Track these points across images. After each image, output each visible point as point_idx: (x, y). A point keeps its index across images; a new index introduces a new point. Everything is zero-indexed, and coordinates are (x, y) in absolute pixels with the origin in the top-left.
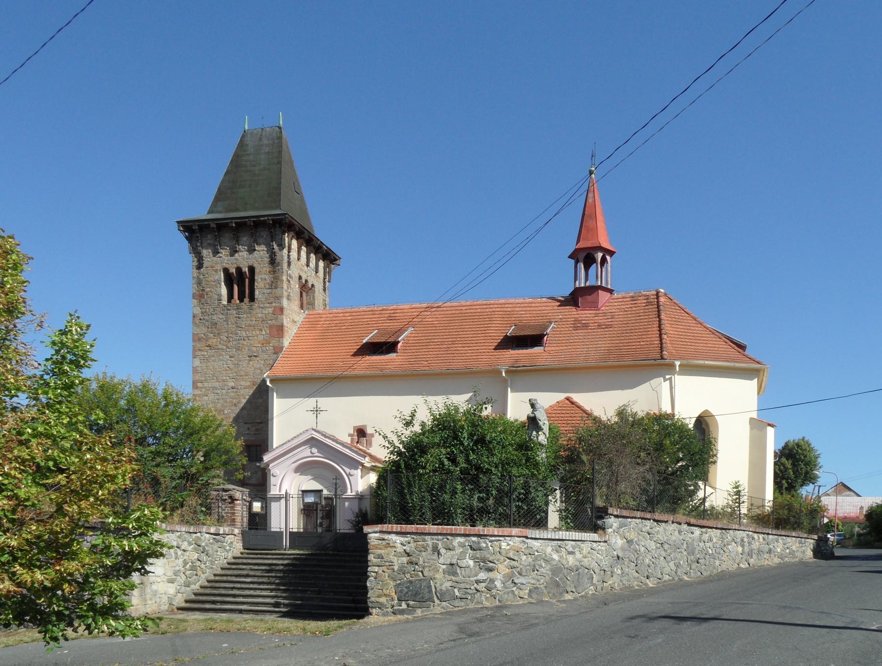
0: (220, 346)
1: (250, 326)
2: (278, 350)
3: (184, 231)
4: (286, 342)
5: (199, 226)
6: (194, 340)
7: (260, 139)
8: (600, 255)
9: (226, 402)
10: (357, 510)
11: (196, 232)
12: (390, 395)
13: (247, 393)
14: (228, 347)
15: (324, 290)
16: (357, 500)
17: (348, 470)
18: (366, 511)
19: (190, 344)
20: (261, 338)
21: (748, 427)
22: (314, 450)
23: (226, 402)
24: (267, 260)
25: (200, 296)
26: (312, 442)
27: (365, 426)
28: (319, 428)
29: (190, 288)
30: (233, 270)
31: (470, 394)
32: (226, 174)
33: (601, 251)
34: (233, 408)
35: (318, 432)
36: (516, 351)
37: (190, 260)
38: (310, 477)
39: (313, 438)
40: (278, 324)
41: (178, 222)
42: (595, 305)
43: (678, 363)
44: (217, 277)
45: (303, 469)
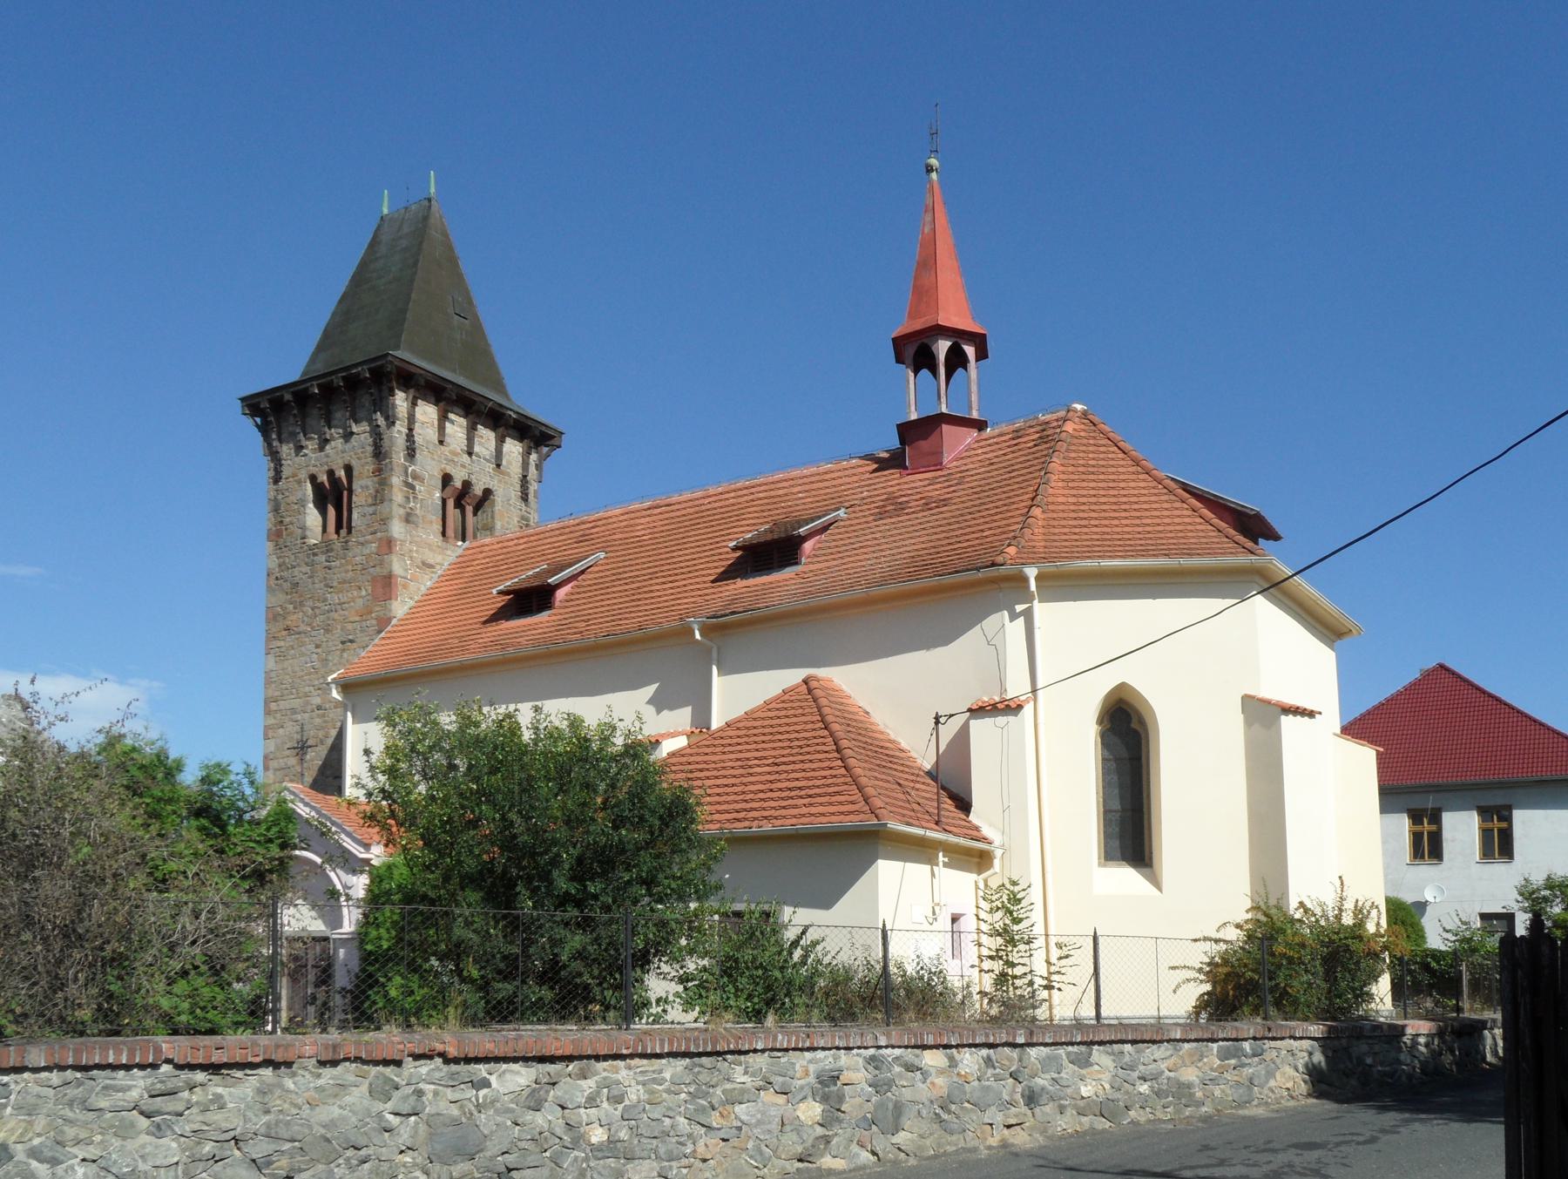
1: (344, 582)
2: (384, 622)
3: (253, 415)
4: (400, 608)
5: (270, 401)
6: (268, 621)
7: (400, 228)
8: (942, 347)
11: (280, 412)
15: (525, 498)
19: (262, 627)
20: (360, 602)
21: (1239, 719)
24: (370, 449)
25: (279, 534)
29: (265, 521)
30: (324, 478)
31: (655, 686)
32: (340, 302)
33: (947, 337)
36: (751, 581)
37: (265, 464)
40: (385, 572)
41: (243, 400)
42: (934, 461)
43: (1031, 572)
44: (299, 495)
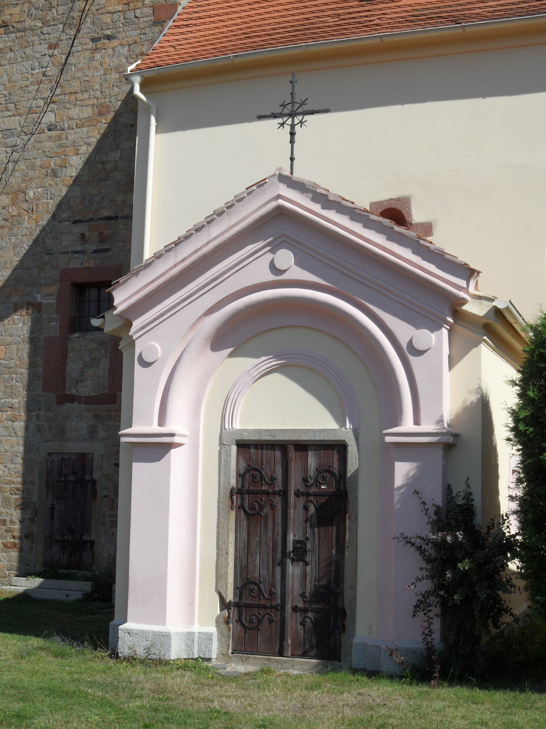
0: (28, 23)
9: (32, 167)
10: (436, 497)
12: (484, 95)
13: (88, 139)
14: (45, 23)
16: (439, 453)
17: (404, 331)
18: (468, 496)
22: (285, 258)
23: (32, 167)
26: (278, 227)
27: (406, 201)
28: (298, 175)
34: (49, 181)
35: (300, 186)
38: (267, 362)
39: (280, 214)
45: (243, 332)
